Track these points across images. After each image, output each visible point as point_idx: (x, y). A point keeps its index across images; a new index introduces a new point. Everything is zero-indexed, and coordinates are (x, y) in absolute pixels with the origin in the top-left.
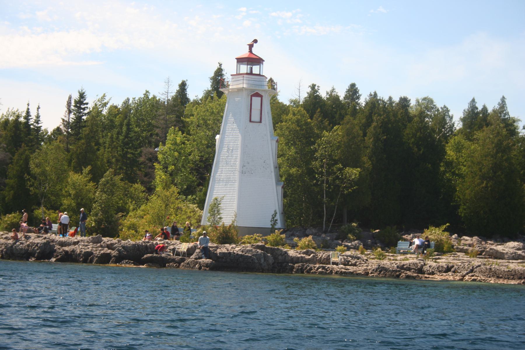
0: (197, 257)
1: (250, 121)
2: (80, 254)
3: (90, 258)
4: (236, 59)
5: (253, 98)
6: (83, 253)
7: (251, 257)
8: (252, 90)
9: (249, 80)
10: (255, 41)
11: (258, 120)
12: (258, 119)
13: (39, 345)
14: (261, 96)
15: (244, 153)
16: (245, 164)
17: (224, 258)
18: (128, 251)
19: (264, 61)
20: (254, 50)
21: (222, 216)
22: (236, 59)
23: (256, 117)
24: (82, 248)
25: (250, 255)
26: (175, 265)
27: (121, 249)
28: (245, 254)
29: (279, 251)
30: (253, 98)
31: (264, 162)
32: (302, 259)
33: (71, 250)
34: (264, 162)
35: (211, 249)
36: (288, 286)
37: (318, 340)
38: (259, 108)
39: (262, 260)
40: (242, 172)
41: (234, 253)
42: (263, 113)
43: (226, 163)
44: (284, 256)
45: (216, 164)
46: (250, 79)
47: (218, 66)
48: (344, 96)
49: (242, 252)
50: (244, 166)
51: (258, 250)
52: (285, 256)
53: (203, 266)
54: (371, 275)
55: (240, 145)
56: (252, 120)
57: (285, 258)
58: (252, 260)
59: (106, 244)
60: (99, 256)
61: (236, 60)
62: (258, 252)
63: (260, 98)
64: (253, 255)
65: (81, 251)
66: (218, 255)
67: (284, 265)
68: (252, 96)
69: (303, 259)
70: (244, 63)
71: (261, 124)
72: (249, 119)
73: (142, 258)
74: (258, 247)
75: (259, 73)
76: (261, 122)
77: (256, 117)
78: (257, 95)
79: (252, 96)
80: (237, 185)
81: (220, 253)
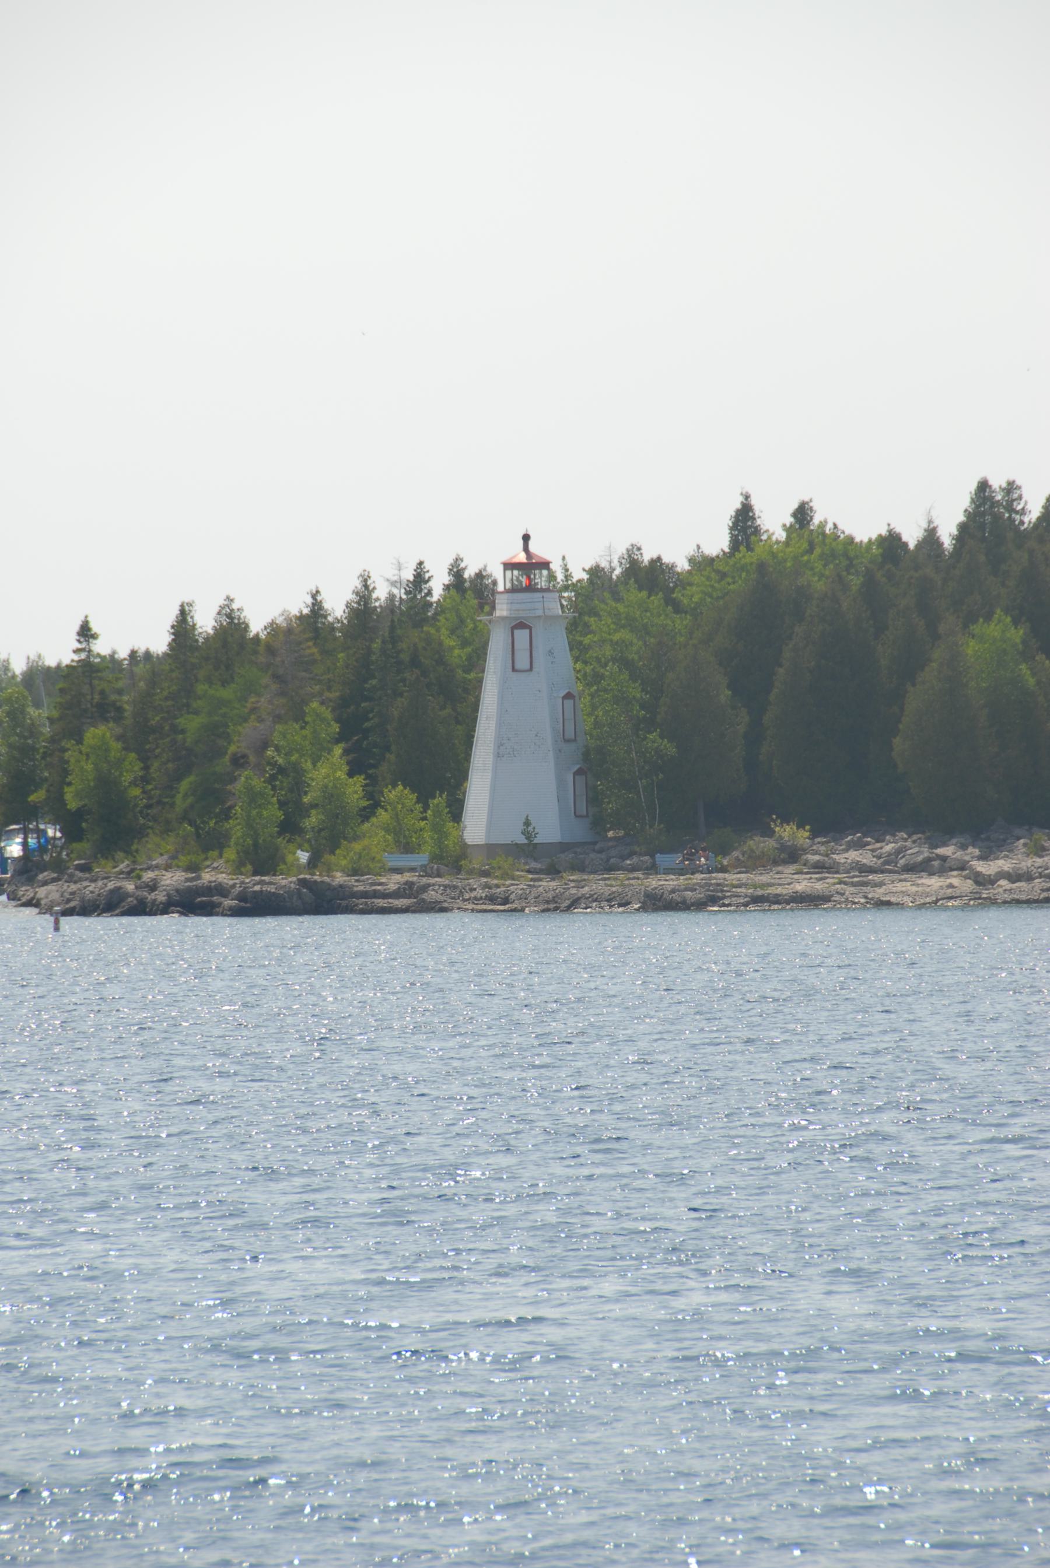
1: (514, 669)
5: (516, 632)
8: (516, 618)
10: (526, 538)
11: (528, 667)
13: (844, 1412)
20: (533, 547)
23: (522, 662)
30: (516, 632)
35: (55, 875)
37: (741, 1123)
38: (528, 646)
40: (498, 756)
47: (741, 499)
48: (961, 518)
56: (518, 666)
61: (502, 567)
63: (527, 631)
68: (513, 628)
70: (539, 560)
76: (531, 669)
77: (522, 662)
78: (521, 625)
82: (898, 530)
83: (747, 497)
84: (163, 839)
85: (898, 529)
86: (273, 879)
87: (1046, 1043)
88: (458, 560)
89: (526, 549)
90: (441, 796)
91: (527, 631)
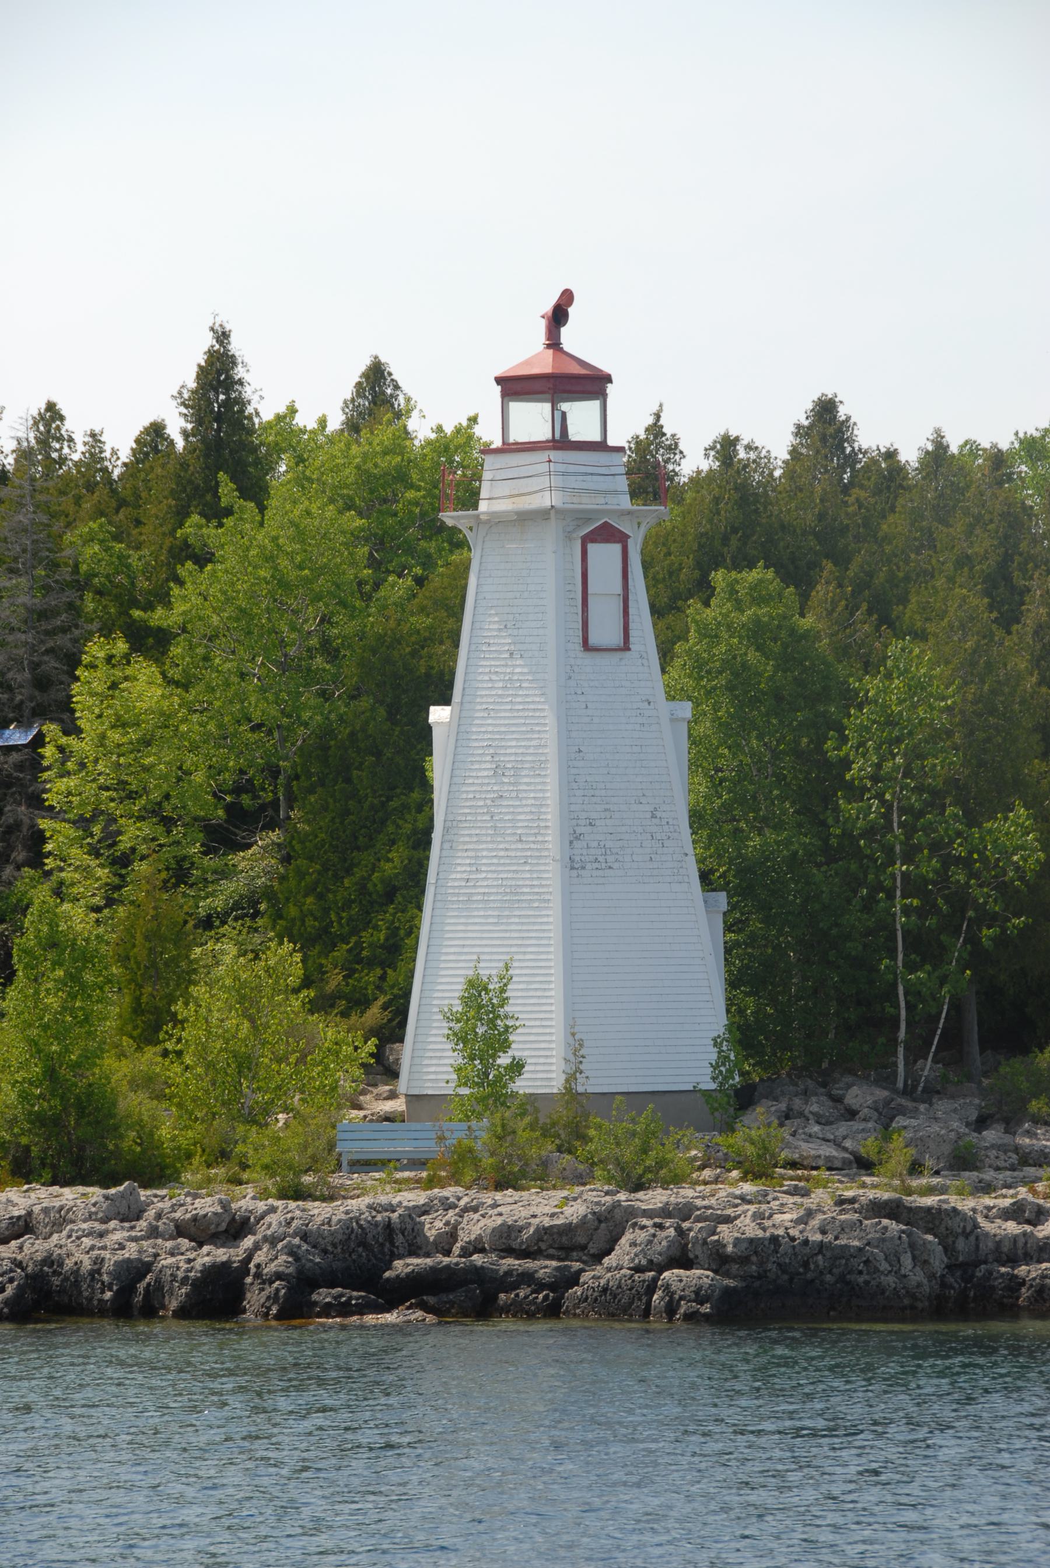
0: (644, 1262)
2: (95, 1273)
3: (141, 1286)
4: (499, 380)
5: (592, 548)
6: (108, 1266)
7: (860, 1250)
8: (582, 517)
9: (564, 474)
10: (558, 316)
11: (617, 639)
12: (615, 638)
14: (622, 539)
15: (570, 784)
16: (579, 830)
17: (754, 1259)
18: (325, 1251)
19: (608, 379)
21: (517, 1050)
22: (499, 380)
24: (92, 1248)
25: (856, 1243)
26: (541, 1296)
27: (299, 1247)
28: (836, 1238)
29: (958, 1219)
30: (592, 548)
31: (653, 816)
32: (1026, 1243)
33: (39, 1257)
34: (653, 816)
36: (288, 1224)
38: (618, 589)
39: (907, 1261)
40: (573, 865)
41: (793, 1239)
42: (631, 611)
43: (495, 828)
44: (972, 1238)
45: (446, 830)
46: (572, 469)
47: (208, 341)
49: (823, 1232)
50: (577, 838)
51: (885, 1222)
52: (977, 1238)
53: (681, 1298)
54: (693, 1153)
55: (551, 751)
56: (593, 640)
57: (977, 1247)
58: (867, 1262)
59: (173, 1220)
60: (196, 1279)
62: (886, 1228)
63: (617, 548)
64: (868, 1244)
65: (99, 1261)
66: (730, 1249)
67: (979, 1274)
68: (586, 540)
69: (1030, 1241)
70: (577, 370)
71: (628, 653)
72: (619, 655)
73: (387, 1274)
74: (878, 1209)
75: (596, 437)
76: (626, 647)
79: (586, 540)
80: (553, 917)
81: (737, 1242)
82: (383, 361)
83: (223, 336)
84: (356, 884)
85: (167, 422)
86: (871, 1194)
87: (4, 1427)
88: (324, 416)
89: (554, 343)
90: (47, 799)
91: (617, 548)
